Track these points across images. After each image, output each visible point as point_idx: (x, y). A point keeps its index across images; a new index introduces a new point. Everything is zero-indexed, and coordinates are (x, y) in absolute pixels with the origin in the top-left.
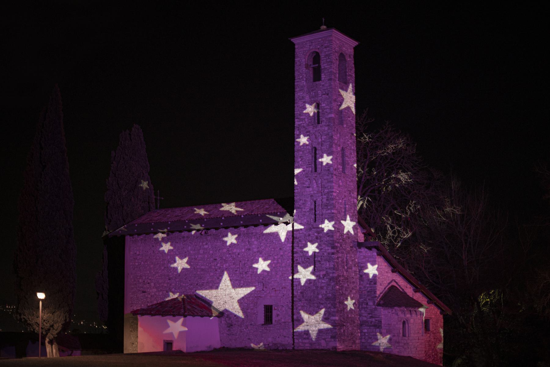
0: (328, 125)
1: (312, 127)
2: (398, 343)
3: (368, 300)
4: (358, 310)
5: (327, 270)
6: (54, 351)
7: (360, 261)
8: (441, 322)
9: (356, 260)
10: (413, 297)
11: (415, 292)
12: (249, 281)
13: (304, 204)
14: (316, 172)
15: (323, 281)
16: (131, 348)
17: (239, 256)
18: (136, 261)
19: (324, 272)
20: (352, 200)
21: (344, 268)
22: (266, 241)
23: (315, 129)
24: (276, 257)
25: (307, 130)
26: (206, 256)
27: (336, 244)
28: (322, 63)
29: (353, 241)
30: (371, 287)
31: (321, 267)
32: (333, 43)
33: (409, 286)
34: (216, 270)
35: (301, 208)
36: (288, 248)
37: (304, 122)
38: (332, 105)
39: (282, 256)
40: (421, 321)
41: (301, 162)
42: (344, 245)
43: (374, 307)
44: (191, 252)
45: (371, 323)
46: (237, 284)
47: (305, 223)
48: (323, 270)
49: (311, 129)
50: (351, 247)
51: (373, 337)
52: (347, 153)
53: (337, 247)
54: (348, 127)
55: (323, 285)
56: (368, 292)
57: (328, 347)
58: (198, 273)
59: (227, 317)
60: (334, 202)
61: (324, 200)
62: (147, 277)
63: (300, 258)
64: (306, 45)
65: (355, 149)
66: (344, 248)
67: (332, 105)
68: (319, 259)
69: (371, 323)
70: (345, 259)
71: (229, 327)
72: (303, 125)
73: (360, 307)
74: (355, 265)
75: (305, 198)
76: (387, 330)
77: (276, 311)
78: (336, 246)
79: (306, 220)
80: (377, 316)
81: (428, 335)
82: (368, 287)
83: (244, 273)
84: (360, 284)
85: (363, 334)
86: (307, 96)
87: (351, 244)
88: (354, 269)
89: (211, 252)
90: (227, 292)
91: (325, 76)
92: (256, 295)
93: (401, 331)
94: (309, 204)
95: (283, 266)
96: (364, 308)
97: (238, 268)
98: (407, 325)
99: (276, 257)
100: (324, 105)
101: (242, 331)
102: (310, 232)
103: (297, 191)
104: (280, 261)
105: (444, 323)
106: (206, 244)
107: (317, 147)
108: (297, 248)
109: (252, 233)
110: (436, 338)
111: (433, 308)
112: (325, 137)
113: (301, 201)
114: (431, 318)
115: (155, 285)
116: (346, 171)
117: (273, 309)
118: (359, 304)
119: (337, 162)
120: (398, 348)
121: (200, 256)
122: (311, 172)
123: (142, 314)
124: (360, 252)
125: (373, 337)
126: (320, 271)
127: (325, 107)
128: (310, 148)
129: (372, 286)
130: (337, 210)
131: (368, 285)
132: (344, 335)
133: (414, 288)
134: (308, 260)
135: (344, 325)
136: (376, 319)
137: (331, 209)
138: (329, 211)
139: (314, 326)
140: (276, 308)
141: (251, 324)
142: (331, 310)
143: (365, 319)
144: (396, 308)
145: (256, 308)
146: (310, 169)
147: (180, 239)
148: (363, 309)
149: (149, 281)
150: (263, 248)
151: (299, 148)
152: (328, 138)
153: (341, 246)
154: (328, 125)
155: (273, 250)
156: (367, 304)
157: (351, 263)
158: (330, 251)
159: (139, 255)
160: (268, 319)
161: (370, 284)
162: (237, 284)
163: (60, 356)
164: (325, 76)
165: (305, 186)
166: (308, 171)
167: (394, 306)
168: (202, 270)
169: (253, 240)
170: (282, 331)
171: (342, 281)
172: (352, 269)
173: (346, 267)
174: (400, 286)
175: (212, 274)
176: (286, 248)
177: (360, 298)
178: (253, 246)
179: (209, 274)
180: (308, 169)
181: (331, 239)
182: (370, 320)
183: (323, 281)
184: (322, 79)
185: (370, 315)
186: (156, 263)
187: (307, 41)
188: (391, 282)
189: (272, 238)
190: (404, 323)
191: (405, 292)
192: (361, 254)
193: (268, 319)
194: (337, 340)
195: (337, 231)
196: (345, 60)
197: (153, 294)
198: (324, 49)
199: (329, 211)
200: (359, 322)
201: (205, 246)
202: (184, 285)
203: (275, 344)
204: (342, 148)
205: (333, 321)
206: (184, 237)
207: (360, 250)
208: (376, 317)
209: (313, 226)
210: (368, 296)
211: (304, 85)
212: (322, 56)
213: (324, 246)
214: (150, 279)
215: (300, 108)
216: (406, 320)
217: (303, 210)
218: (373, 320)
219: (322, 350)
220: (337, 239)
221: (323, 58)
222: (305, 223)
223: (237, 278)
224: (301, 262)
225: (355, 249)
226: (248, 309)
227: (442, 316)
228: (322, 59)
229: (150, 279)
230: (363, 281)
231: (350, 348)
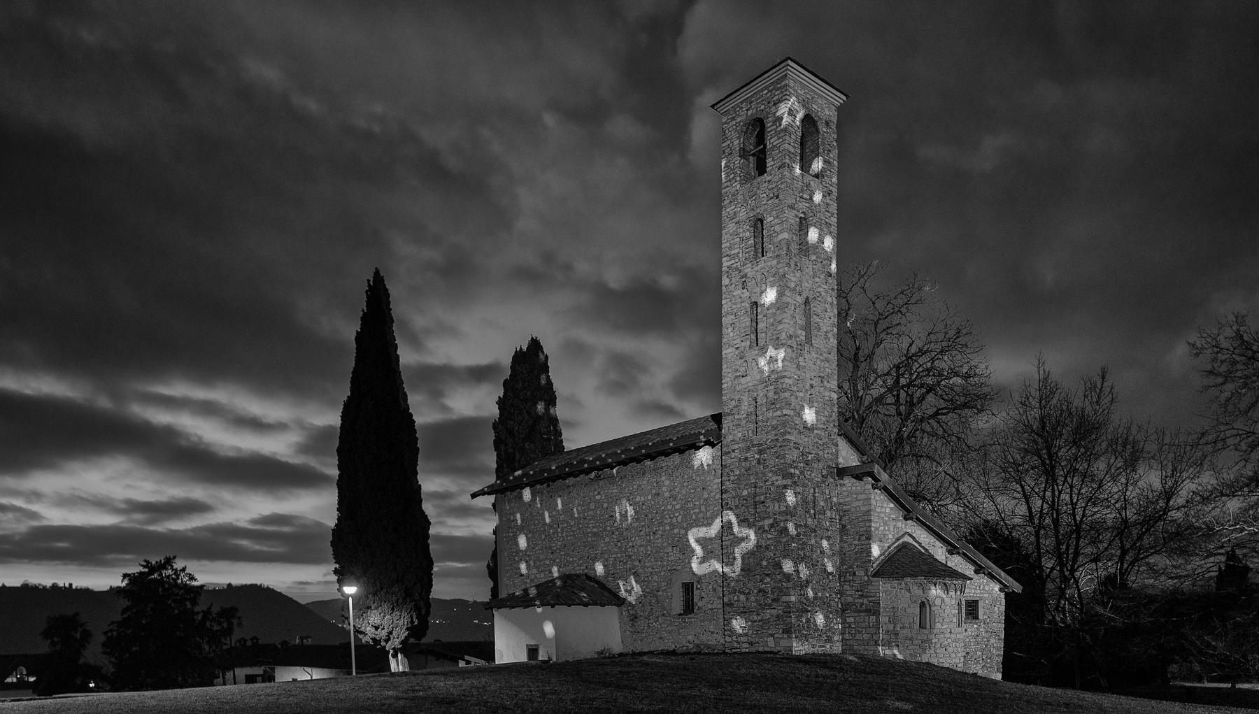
2: (911, 639)
3: (855, 566)
4: (838, 584)
5: (775, 517)
7: (841, 501)
8: (1001, 604)
9: (835, 499)
10: (946, 562)
11: (951, 553)
12: (659, 545)
13: (737, 406)
15: (770, 536)
17: (644, 507)
18: (510, 530)
19: (771, 521)
20: (827, 394)
21: (808, 512)
23: (756, 269)
24: (697, 503)
25: (742, 274)
26: (599, 512)
27: (792, 471)
28: (769, 138)
29: (828, 466)
30: (862, 545)
31: (766, 512)
32: (790, 92)
33: (938, 544)
34: (613, 533)
35: (732, 414)
36: (715, 486)
37: (737, 260)
38: (785, 215)
39: (706, 500)
40: (957, 602)
41: (731, 334)
42: (809, 473)
43: (866, 578)
45: (861, 606)
46: (643, 552)
47: (740, 438)
48: (769, 517)
49: (749, 269)
50: (823, 476)
51: (864, 630)
52: (816, 307)
53: (792, 475)
54: (820, 260)
55: (768, 543)
56: (856, 553)
57: (778, 649)
58: (589, 539)
60: (787, 395)
61: (771, 394)
63: (733, 500)
64: (741, 111)
65: (835, 303)
66: (807, 477)
67: (785, 215)
68: (762, 498)
69: (861, 606)
70: (810, 497)
71: (632, 620)
72: (735, 265)
73: (842, 580)
74: (832, 508)
75: (739, 396)
76: (889, 618)
77: (699, 591)
78: (791, 474)
79: (740, 434)
80: (872, 595)
81: (975, 626)
82: (856, 545)
83: (651, 534)
84: (841, 541)
85: (847, 625)
86: (743, 210)
87: (823, 471)
88: (828, 514)
89: (605, 505)
90: (628, 566)
91: (773, 163)
92: (669, 568)
93: (917, 620)
95: (708, 516)
96: (849, 581)
98: (928, 608)
99: (697, 503)
101: (651, 625)
102: (748, 454)
103: (726, 385)
104: (703, 508)
105: (1005, 606)
106: (599, 494)
108: (728, 483)
110: (991, 630)
111: (985, 581)
112: (773, 279)
113: (733, 401)
114: (981, 598)
115: (535, 564)
116: (813, 342)
117: (695, 588)
118: (839, 575)
119: (795, 323)
120: (910, 647)
121: (591, 513)
122: (750, 348)
124: (841, 485)
125: (864, 630)
126: (764, 519)
127: (773, 222)
128: (747, 305)
129: (863, 542)
130: (792, 410)
131: (856, 542)
132: (808, 628)
133: (949, 548)
134: (745, 502)
135: (808, 611)
136: (870, 599)
137: (781, 408)
138: (779, 413)
139: (755, 613)
140: (699, 586)
141: (663, 615)
142: (782, 585)
143: (850, 599)
144: (908, 579)
145: (670, 588)
146: (748, 343)
147: (564, 490)
148: (848, 583)
150: (677, 490)
151: (729, 309)
152: (777, 281)
153: (802, 472)
154: (778, 256)
155: (692, 491)
156: (854, 574)
157: (822, 503)
158: (779, 482)
160: (689, 607)
162: (643, 552)
163: (1011, 667)
164: (773, 163)
165: (738, 374)
166: (745, 347)
168: (595, 534)
169: (663, 478)
170: (707, 623)
171: (804, 535)
172: (825, 514)
173: (812, 511)
174: (920, 544)
175: (607, 540)
176: (711, 487)
177: (842, 563)
178: (664, 489)
180: (743, 344)
181: (782, 461)
182: (860, 601)
183: (770, 536)
184: (768, 170)
185: (860, 593)
186: (535, 531)
188: (903, 536)
189: (691, 472)
190: (922, 605)
191: (930, 553)
192: (845, 489)
193: (689, 607)
194: (794, 636)
195: (794, 447)
196: (817, 131)
197: (533, 577)
198: (771, 109)
199: (779, 413)
200: (840, 606)
201: (598, 497)
202: (571, 560)
203: (698, 646)
204: (807, 298)
205: (785, 604)
206: (569, 486)
207: (842, 482)
208: (871, 597)
210: (856, 559)
211: (737, 191)
213: (770, 475)
216: (925, 601)
217: (737, 417)
218: (865, 601)
219: (766, 652)
220: (794, 462)
221: (771, 126)
222: (740, 438)
223: (642, 543)
224: (734, 507)
225: (832, 480)
226: (658, 591)
227: (1002, 595)
228: (769, 130)
230: (847, 535)
231: (820, 651)
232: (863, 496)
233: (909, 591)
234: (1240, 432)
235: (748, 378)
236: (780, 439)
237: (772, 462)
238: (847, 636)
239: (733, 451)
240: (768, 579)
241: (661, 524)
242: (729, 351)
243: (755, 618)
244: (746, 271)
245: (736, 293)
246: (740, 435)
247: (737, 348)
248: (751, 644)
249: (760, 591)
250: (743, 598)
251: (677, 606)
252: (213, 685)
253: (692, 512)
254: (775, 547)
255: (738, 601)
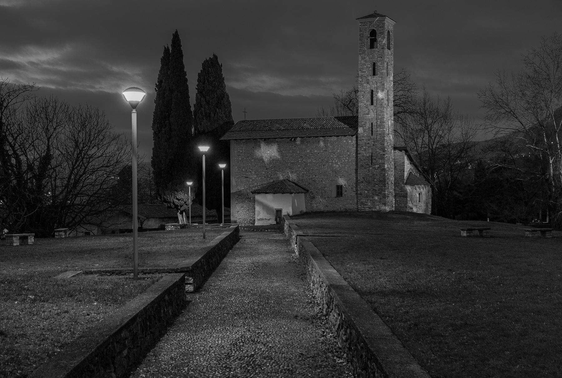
0: (381, 77)
1: (370, 77)
6: (184, 219)
13: (365, 124)
14: (373, 105)
15: (378, 171)
16: (237, 215)
17: (319, 155)
19: (378, 166)
22: (338, 146)
23: (373, 79)
44: (284, 152)
55: (377, 173)
56: (400, 176)
58: (289, 165)
59: (310, 193)
61: (379, 123)
62: (249, 168)
68: (375, 158)
89: (298, 152)
94: (368, 125)
97: (318, 162)
99: (345, 156)
100: (379, 64)
104: (347, 158)
106: (295, 147)
107: (374, 90)
109: (328, 141)
123: (259, 193)
126: (376, 165)
131: (400, 173)
138: (382, 130)
143: (397, 192)
144: (416, 186)
149: (250, 170)
154: (381, 77)
158: (382, 153)
159: (242, 153)
161: (401, 172)
167: (415, 185)
168: (292, 163)
175: (299, 166)
179: (297, 166)
180: (367, 103)
183: (378, 171)
187: (368, 22)
199: (382, 130)
201: (294, 148)
209: (371, 137)
210: (400, 178)
212: (378, 32)
213: (378, 150)
214: (251, 169)
215: (363, 64)
218: (403, 193)
229: (251, 169)
232: (402, 157)
233: (416, 189)
234: (493, 126)
235: (369, 115)
236: (382, 139)
237: (379, 146)
238: (396, 205)
239: (363, 140)
240: (377, 186)
241: (327, 162)
242: (361, 104)
243: (371, 199)
244: (369, 78)
245: (364, 85)
246: (366, 134)
247: (365, 104)
248: (370, 208)
249: (374, 190)
250: (366, 192)
251: (334, 194)
252: (454, 219)
253: (342, 159)
254: (380, 175)
255: (364, 193)
